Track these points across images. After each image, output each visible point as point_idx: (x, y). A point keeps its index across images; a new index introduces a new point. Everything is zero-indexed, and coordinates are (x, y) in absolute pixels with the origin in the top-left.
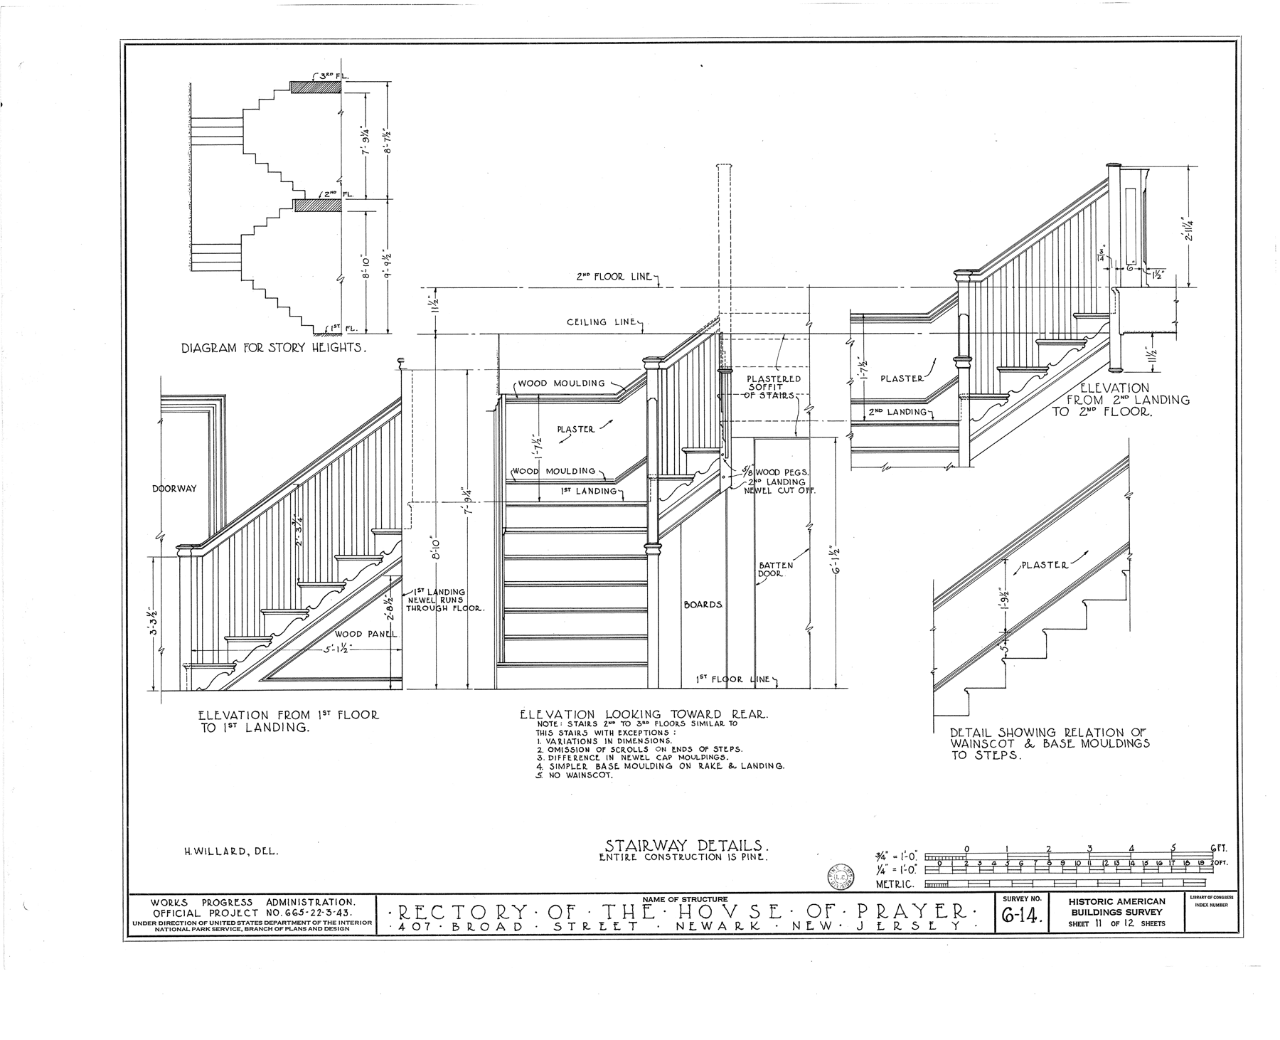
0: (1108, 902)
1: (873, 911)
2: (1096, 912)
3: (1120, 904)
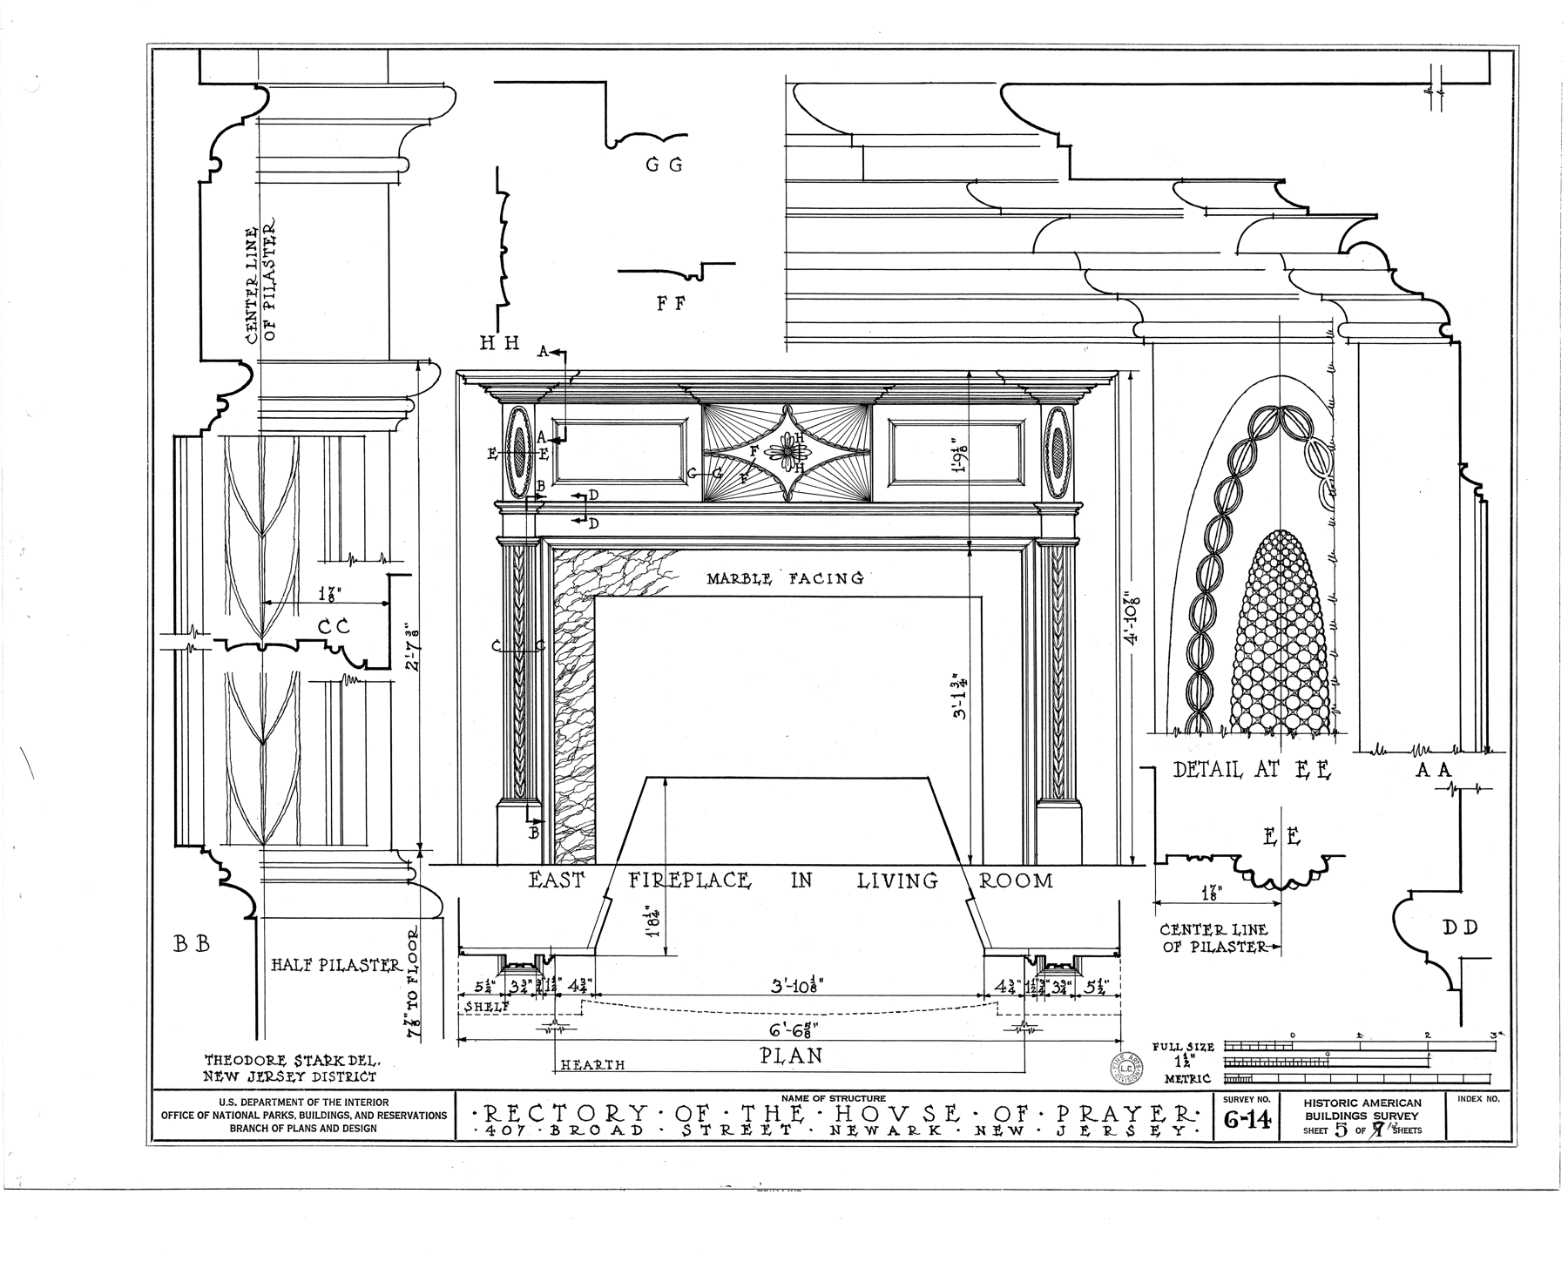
0: (1350, 1103)
2: (1336, 1116)
3: (1366, 1106)
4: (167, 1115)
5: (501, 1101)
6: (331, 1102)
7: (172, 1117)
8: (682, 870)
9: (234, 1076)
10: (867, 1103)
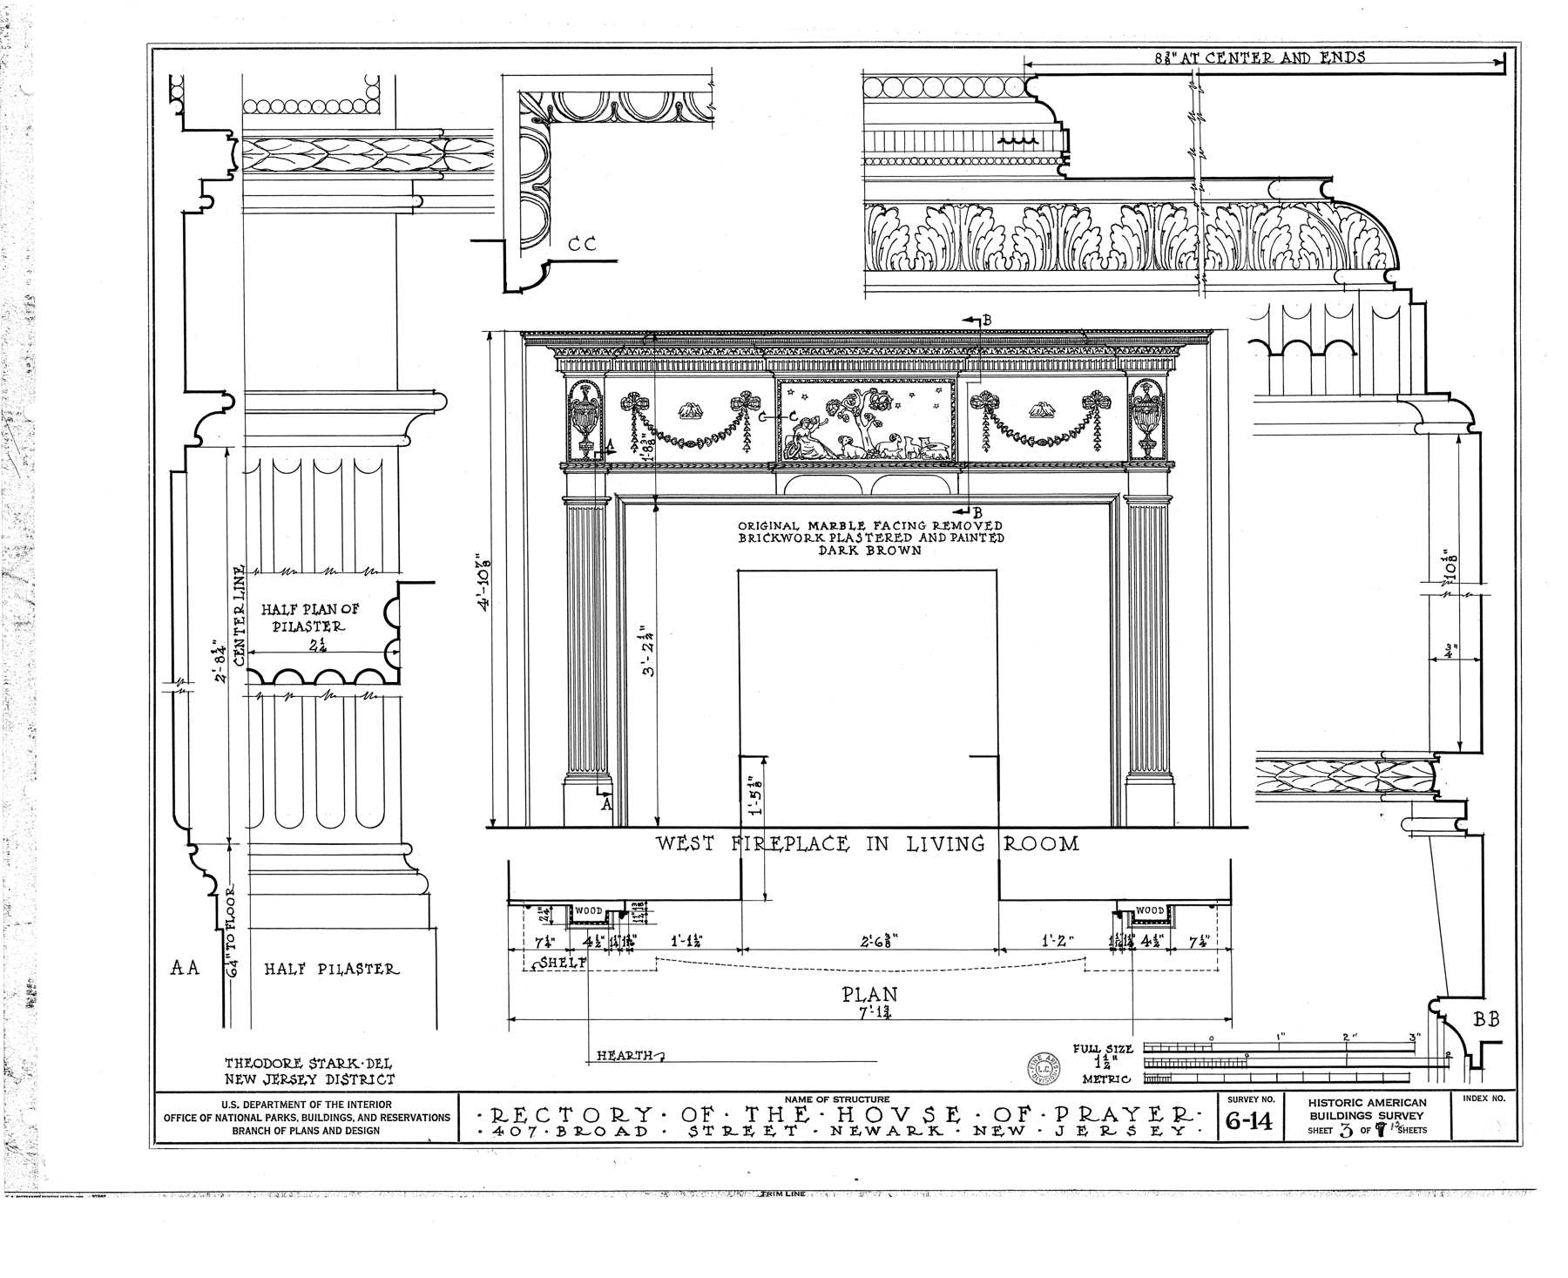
0: (1356, 1103)
1: (1075, 1115)
2: (1341, 1116)
3: (1371, 1105)
4: (169, 1118)
5: (507, 1104)
6: (333, 1104)
7: (175, 1120)
8: (783, 833)
9: (252, 1079)
10: (871, 1104)
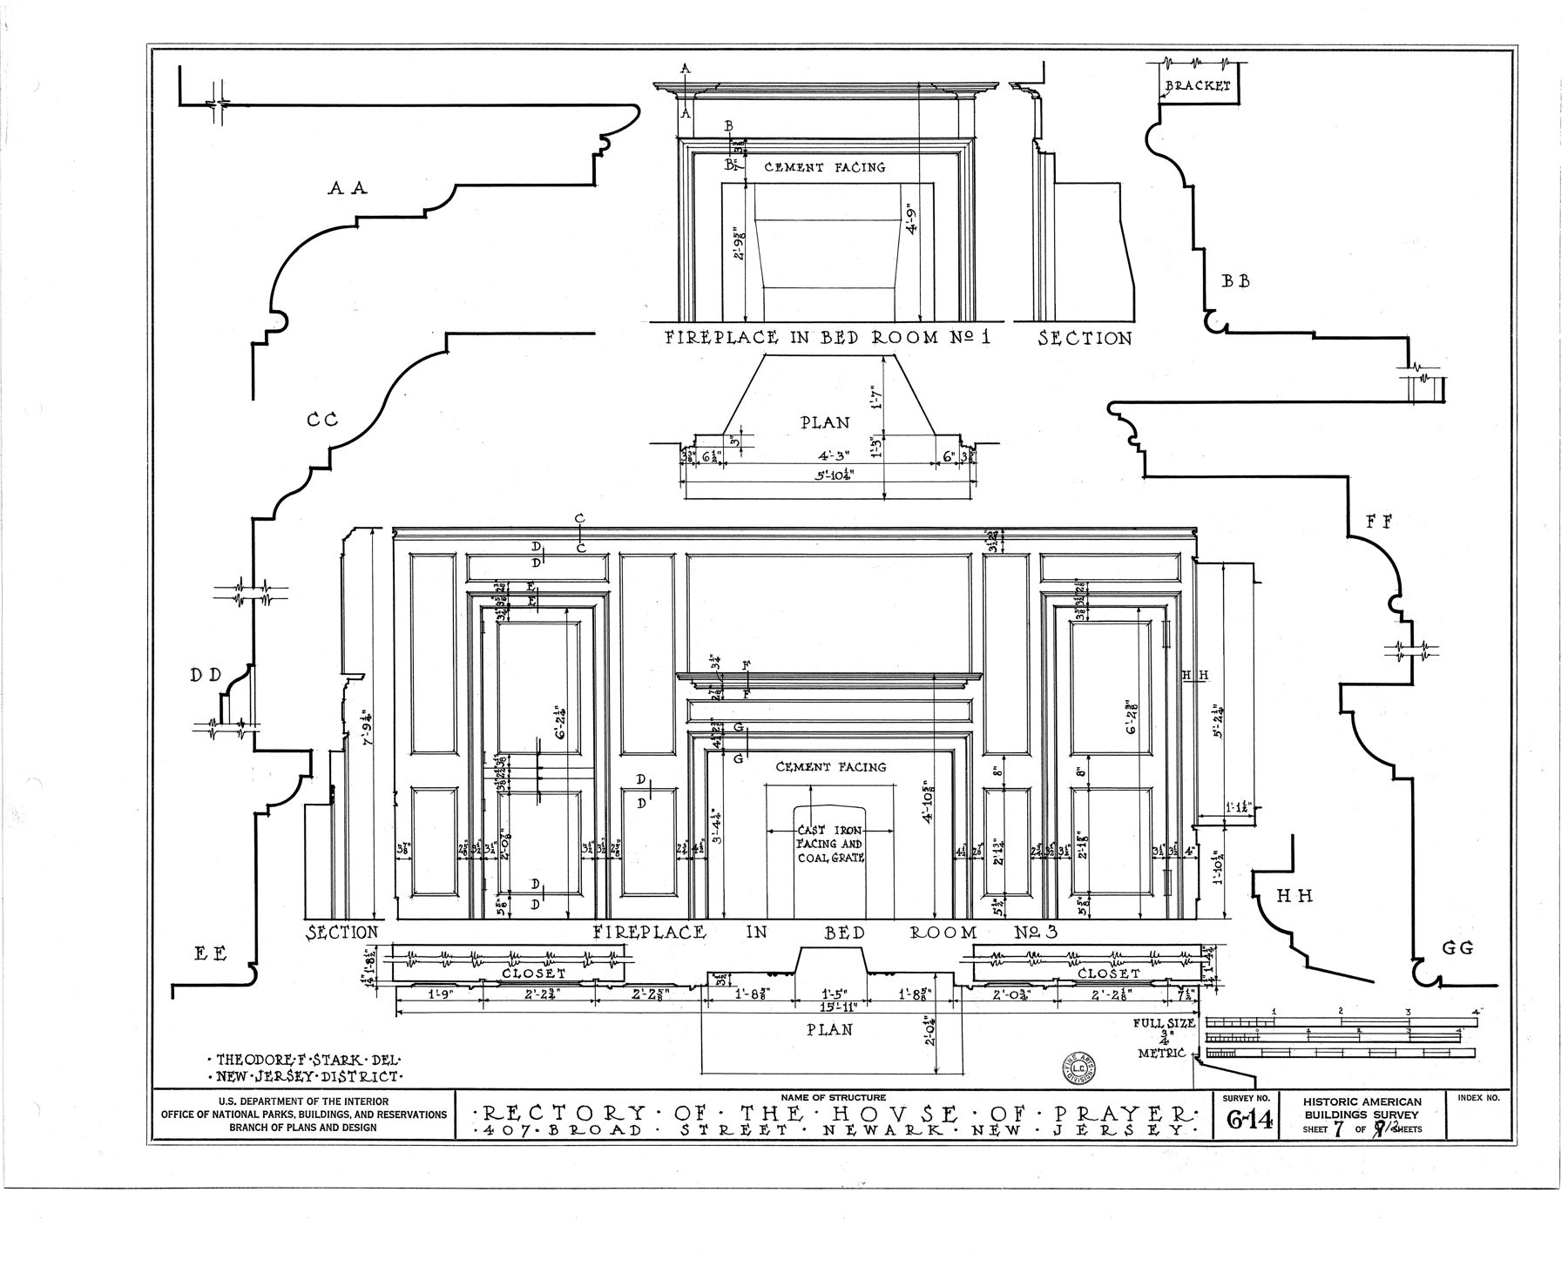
0: (1351, 1102)
2: (1336, 1115)
3: (1366, 1105)
